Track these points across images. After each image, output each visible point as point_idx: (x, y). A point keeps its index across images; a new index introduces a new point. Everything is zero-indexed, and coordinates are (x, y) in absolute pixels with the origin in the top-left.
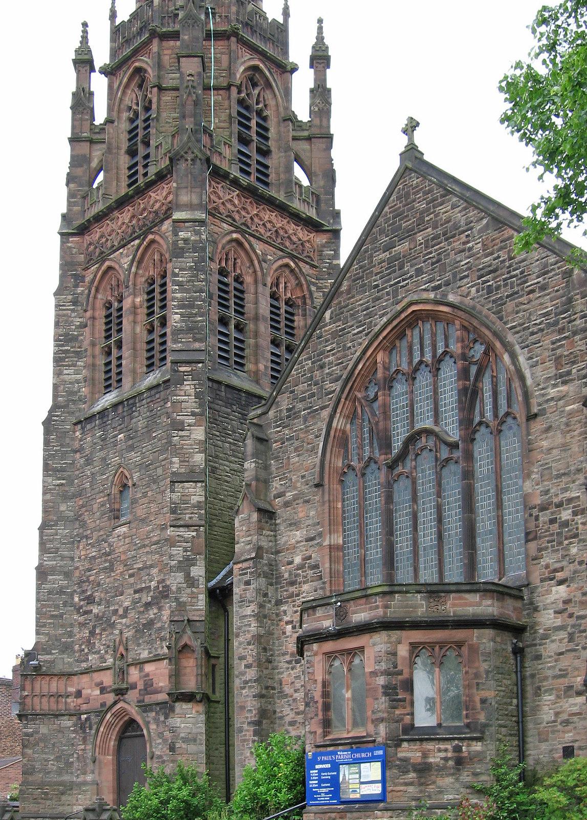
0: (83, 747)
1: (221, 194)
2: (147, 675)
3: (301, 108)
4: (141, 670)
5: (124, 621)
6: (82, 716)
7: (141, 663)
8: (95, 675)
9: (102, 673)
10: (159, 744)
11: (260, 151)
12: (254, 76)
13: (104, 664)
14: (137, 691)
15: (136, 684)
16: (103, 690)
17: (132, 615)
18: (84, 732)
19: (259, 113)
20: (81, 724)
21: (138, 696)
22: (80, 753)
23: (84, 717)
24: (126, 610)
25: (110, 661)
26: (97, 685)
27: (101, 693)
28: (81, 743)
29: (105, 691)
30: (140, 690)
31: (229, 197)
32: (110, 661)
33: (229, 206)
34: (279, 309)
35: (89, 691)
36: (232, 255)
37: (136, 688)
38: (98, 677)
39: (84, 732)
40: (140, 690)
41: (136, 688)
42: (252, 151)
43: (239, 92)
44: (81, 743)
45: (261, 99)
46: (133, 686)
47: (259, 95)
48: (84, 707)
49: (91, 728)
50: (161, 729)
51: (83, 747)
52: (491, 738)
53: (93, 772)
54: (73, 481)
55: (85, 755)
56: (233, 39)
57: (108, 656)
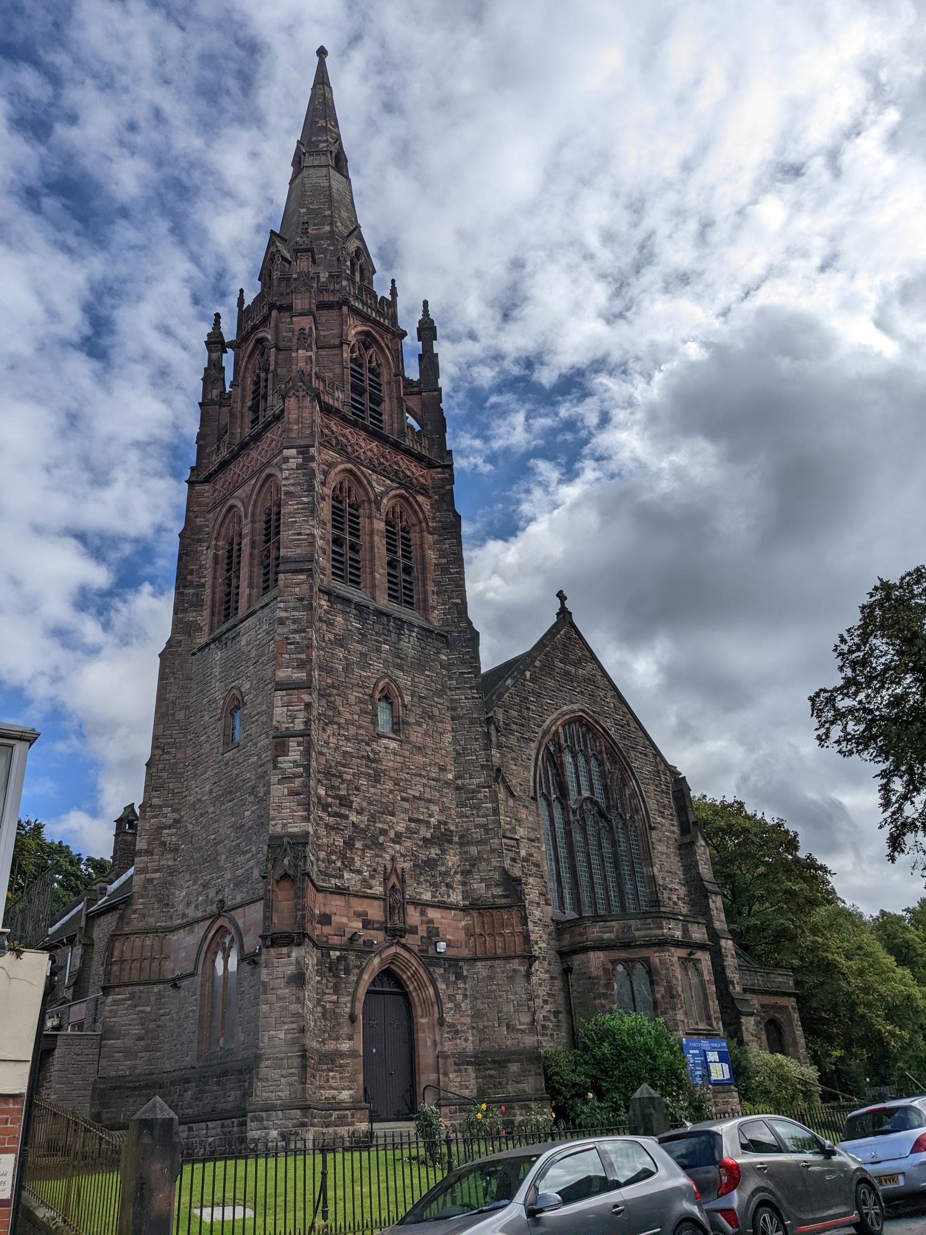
0: (334, 998)
1: (363, 444)
2: (431, 921)
3: (413, 372)
4: (423, 913)
5: (397, 847)
6: (332, 953)
7: (422, 906)
8: (354, 901)
9: (366, 901)
10: (451, 1009)
11: (372, 401)
12: (367, 341)
13: (369, 891)
14: (418, 937)
15: (416, 927)
16: (367, 924)
17: (409, 844)
18: (336, 976)
19: (371, 371)
20: (331, 963)
21: (419, 943)
22: (328, 1006)
23: (335, 954)
24: (398, 835)
25: (378, 890)
26: (358, 915)
27: (365, 927)
28: (331, 991)
29: (370, 927)
30: (422, 937)
31: (369, 447)
32: (378, 890)
33: (369, 453)
34: (403, 556)
35: (345, 920)
36: (346, 485)
37: (416, 933)
38: (360, 905)
39: (336, 976)
40: (422, 937)
41: (416, 933)
42: (366, 399)
43: (352, 352)
44: (331, 991)
45: (374, 359)
46: (414, 930)
47: (371, 356)
48: (335, 940)
49: (347, 972)
50: (451, 992)
51: (334, 998)
52: (894, 607)
53: (350, 1038)
54: (869, 720)
55: (337, 1010)
56: (345, 309)
57: (373, 882)
